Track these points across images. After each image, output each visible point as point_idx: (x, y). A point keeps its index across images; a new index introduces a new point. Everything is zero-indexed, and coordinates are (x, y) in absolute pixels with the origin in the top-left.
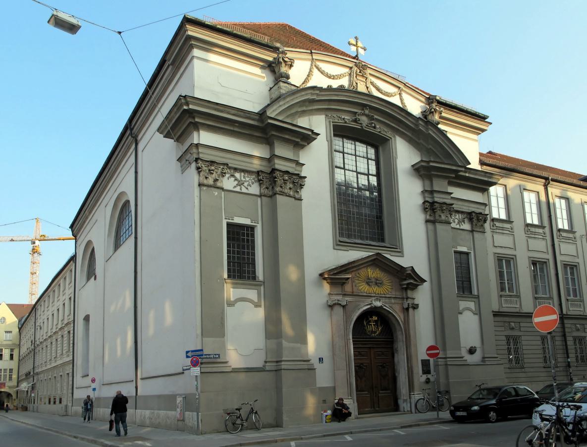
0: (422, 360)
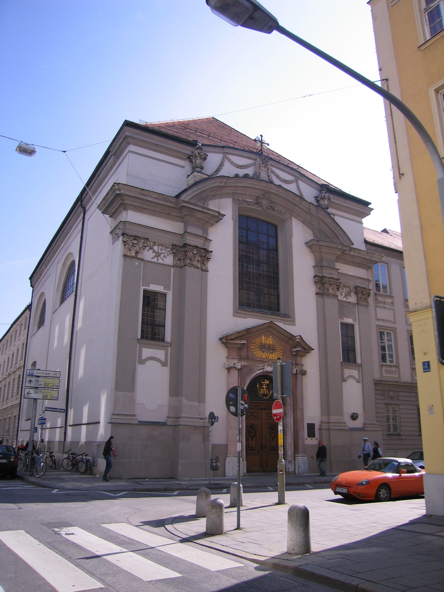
0: (308, 424)
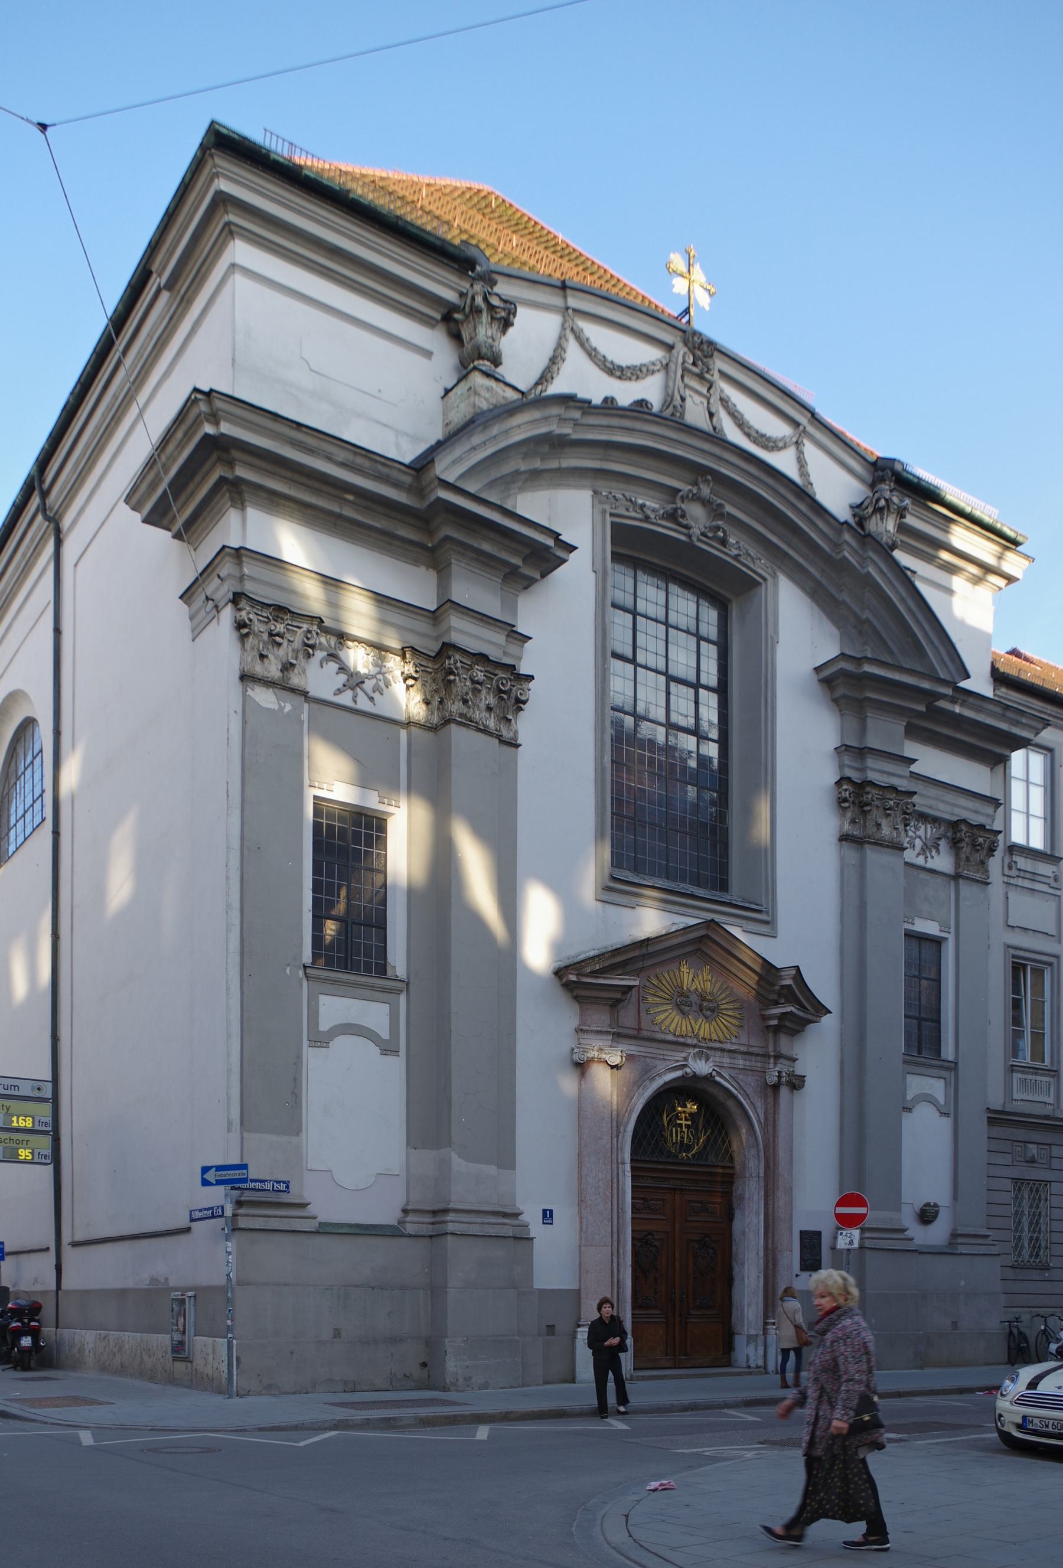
0: (801, 1232)
